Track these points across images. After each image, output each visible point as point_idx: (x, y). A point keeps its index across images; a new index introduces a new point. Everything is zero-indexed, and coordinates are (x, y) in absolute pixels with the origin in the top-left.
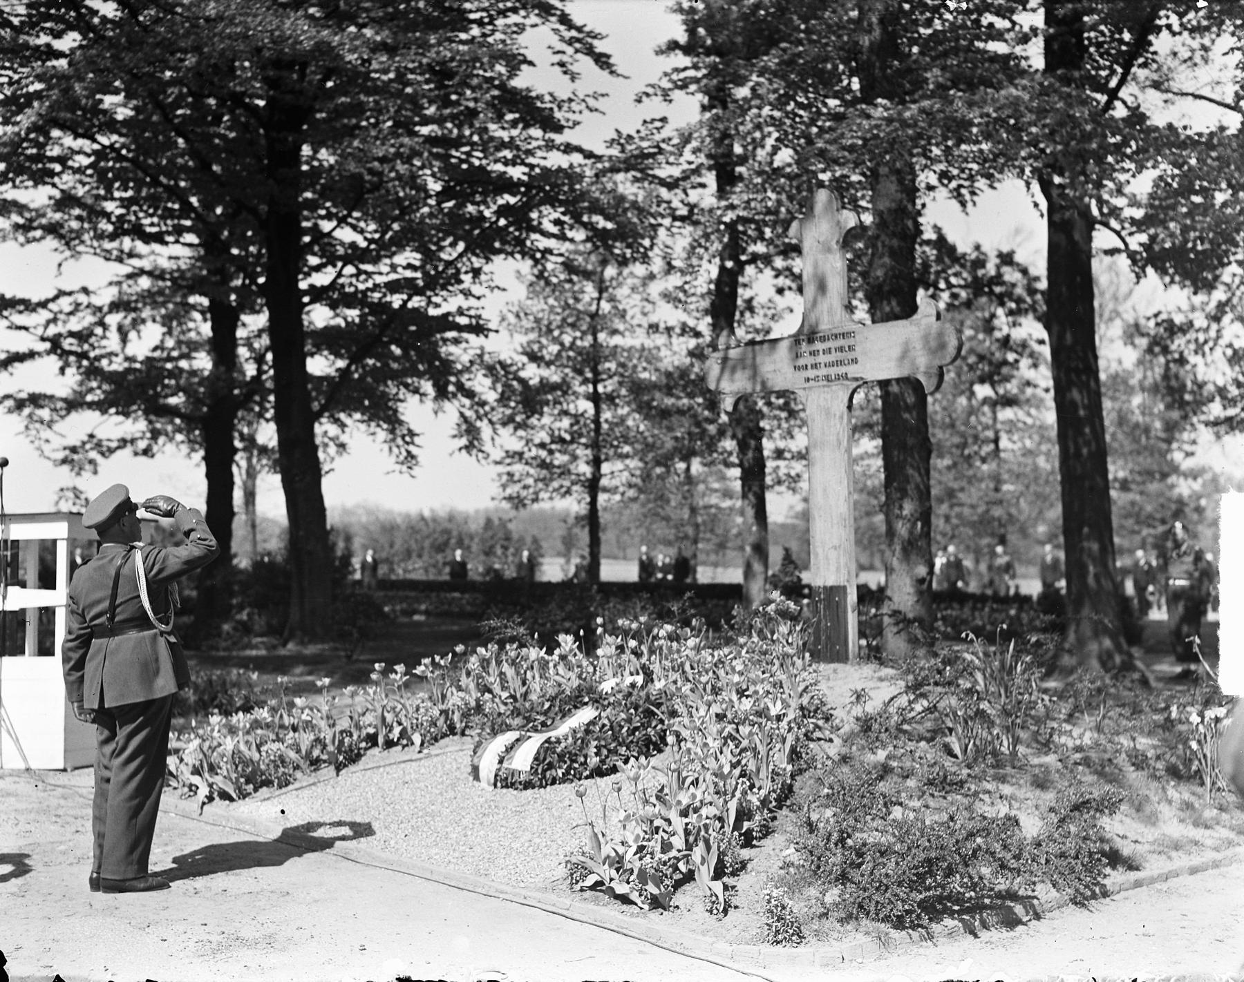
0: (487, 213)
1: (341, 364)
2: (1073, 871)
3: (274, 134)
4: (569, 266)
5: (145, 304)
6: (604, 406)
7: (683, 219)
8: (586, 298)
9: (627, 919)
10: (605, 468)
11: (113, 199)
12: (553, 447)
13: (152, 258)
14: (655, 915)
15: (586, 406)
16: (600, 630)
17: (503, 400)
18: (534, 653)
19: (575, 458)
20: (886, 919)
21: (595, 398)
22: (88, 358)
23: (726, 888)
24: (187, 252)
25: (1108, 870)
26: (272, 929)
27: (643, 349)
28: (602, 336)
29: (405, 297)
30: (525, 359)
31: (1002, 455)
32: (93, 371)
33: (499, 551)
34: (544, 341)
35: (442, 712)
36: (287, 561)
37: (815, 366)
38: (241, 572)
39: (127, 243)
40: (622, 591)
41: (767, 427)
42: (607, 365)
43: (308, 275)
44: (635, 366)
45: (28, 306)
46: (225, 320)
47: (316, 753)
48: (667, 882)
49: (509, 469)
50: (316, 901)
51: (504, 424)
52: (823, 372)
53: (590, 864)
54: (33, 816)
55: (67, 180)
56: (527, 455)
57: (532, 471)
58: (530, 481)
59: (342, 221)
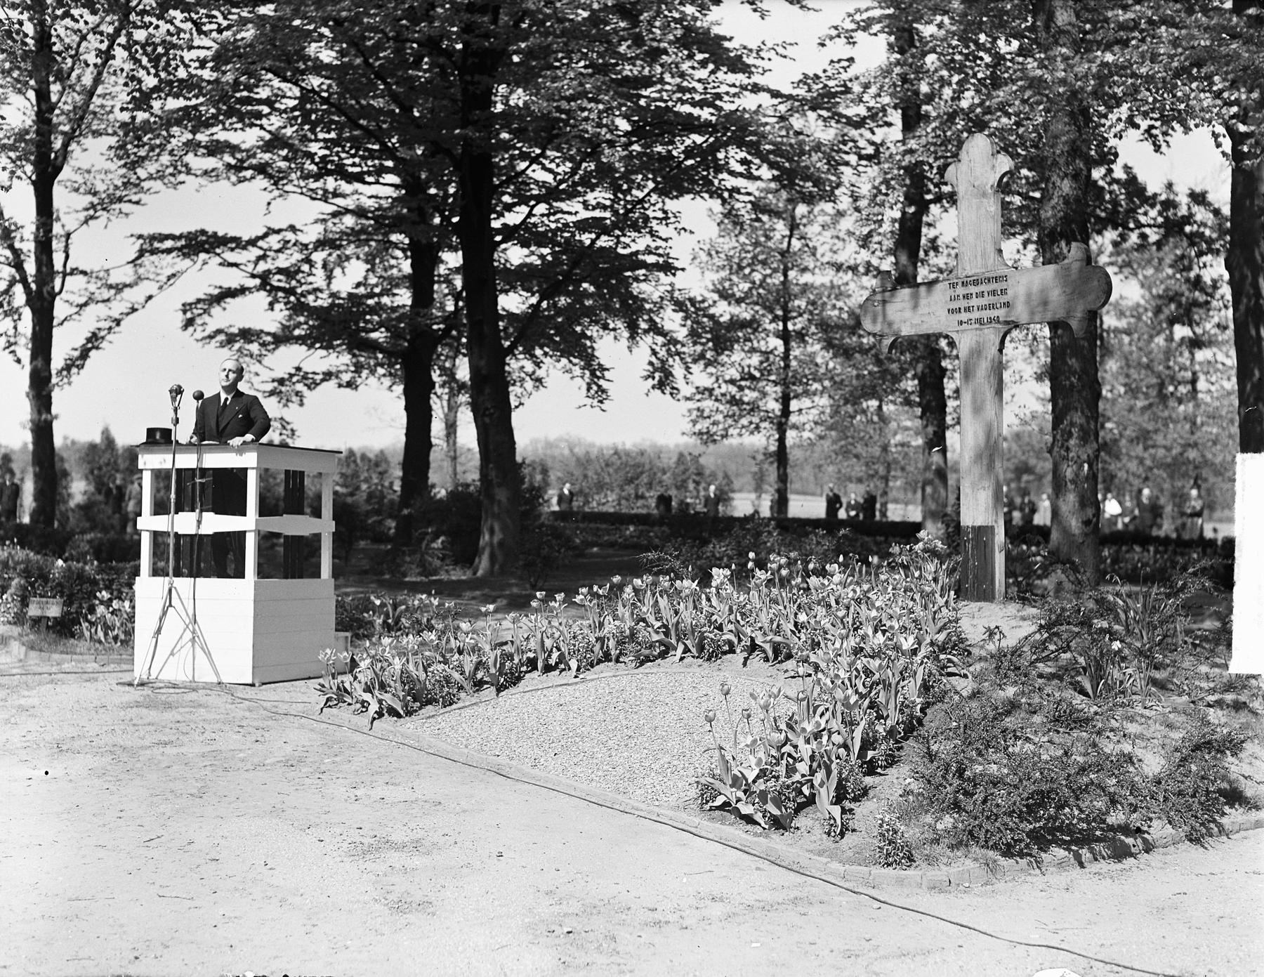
0: (675, 153)
1: (534, 300)
2: (1189, 808)
3: (468, 78)
4: (758, 207)
5: (350, 242)
6: (793, 344)
7: (869, 158)
8: (778, 236)
9: (750, 838)
10: (794, 405)
11: (317, 140)
12: (743, 383)
13: (356, 196)
14: (775, 836)
15: (776, 344)
16: (750, 565)
17: (694, 335)
18: (688, 585)
19: (764, 394)
20: (995, 847)
21: (785, 336)
22: (294, 294)
23: (844, 811)
24: (390, 191)
25: (1227, 809)
26: (421, 834)
27: (832, 287)
28: (792, 274)
29: (593, 236)
30: (716, 297)
31: (1200, 396)
32: (299, 308)
33: (691, 486)
34: (734, 278)
35: (597, 639)
36: (479, 492)
37: (968, 309)
38: (441, 500)
39: (331, 183)
40: (806, 526)
41: (950, 367)
42: (797, 303)
43: (501, 215)
44: (824, 304)
45: (237, 243)
46: (425, 259)
47: (479, 675)
48: (791, 805)
49: (699, 404)
50: (464, 811)
51: (695, 361)
52: (975, 315)
53: (717, 784)
54: (217, 726)
55: (275, 122)
56: (717, 392)
57: (721, 408)
58: (720, 417)
59: (535, 160)
